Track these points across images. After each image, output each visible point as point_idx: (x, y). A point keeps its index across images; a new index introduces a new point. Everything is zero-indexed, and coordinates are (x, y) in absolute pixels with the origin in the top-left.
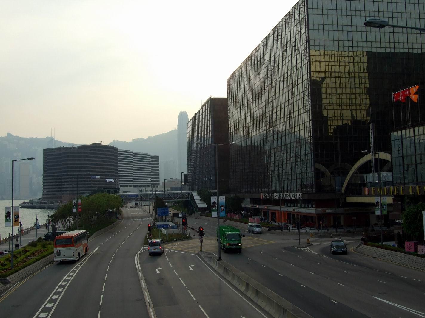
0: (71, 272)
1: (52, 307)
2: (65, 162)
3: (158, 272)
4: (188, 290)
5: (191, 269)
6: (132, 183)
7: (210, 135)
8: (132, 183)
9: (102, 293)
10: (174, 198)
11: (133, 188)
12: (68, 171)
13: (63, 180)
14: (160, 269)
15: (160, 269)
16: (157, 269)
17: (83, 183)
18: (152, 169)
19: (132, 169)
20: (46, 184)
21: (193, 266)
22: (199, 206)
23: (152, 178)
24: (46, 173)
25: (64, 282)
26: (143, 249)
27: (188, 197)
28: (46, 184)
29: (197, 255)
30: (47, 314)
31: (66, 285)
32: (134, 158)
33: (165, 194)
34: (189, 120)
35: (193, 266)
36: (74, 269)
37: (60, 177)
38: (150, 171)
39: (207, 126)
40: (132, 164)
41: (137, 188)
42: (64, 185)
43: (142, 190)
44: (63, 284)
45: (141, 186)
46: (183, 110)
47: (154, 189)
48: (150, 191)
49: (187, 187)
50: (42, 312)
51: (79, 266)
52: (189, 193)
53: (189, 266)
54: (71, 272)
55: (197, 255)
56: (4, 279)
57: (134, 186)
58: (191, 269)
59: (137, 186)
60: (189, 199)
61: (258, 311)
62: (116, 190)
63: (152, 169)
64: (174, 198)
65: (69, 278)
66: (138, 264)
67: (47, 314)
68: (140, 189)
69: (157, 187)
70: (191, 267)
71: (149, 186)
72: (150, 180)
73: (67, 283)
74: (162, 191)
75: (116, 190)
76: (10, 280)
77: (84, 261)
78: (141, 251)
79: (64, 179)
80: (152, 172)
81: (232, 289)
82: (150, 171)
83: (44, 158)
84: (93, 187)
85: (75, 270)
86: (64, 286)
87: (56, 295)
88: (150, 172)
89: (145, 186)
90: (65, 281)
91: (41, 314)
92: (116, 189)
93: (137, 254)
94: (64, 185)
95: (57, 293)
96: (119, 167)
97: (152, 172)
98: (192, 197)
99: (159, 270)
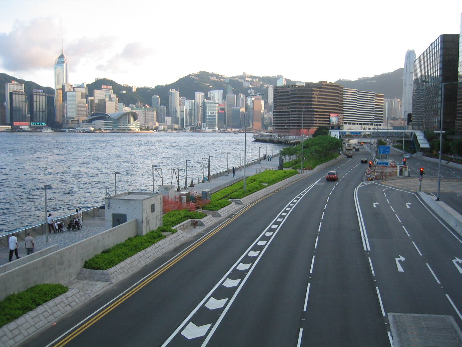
0: (299, 196)
1: (290, 210)
2: (292, 99)
3: (375, 206)
4: (403, 227)
5: (408, 207)
6: (356, 121)
7: (438, 74)
8: (356, 121)
9: (313, 252)
10: (382, 137)
11: (356, 125)
12: (295, 108)
13: (291, 116)
14: (377, 203)
15: (377, 203)
16: (374, 204)
17: (310, 119)
18: (376, 108)
19: (356, 109)
20: (275, 119)
21: (410, 204)
22: (421, 146)
23: (375, 116)
24: (276, 109)
25: (274, 224)
26: (363, 184)
27: (411, 137)
28: (275, 119)
29: (415, 194)
30: (277, 225)
31: (281, 222)
32: (358, 96)
33: (387, 133)
34: (417, 58)
35: (410, 204)
36: (294, 200)
37: (289, 113)
38: (374, 109)
39: (433, 66)
40: (356, 100)
41: (360, 125)
42: (292, 120)
43: (364, 128)
44: (294, 201)
45: (364, 124)
46: (411, 49)
47: (376, 127)
48: (373, 129)
49: (411, 127)
50: (274, 224)
51: (302, 195)
52: (412, 133)
53: (406, 204)
54: (299, 196)
55: (415, 194)
56: (238, 201)
57: (357, 124)
58: (408, 207)
59: (360, 124)
60: (412, 139)
61: (426, 207)
62: (340, 127)
63: (376, 108)
64: (397, 136)
65: (281, 220)
66: (356, 198)
67: (277, 225)
68: (363, 126)
69: (380, 125)
70: (408, 205)
71: (372, 125)
72: (374, 119)
73: (282, 219)
74: (385, 130)
75: (340, 127)
76: (243, 202)
77: (307, 191)
78: (360, 186)
79: (292, 114)
80: (376, 111)
81: (449, 230)
82: (374, 109)
83: (274, 95)
84: (318, 123)
85: (298, 198)
86: (274, 230)
87: (276, 225)
88: (374, 110)
89: (368, 124)
90: (275, 223)
91: (283, 213)
92: (339, 126)
93: (356, 189)
94: (292, 120)
95: (276, 223)
96: (343, 105)
97: (376, 111)
98: (415, 137)
99: (376, 205)
